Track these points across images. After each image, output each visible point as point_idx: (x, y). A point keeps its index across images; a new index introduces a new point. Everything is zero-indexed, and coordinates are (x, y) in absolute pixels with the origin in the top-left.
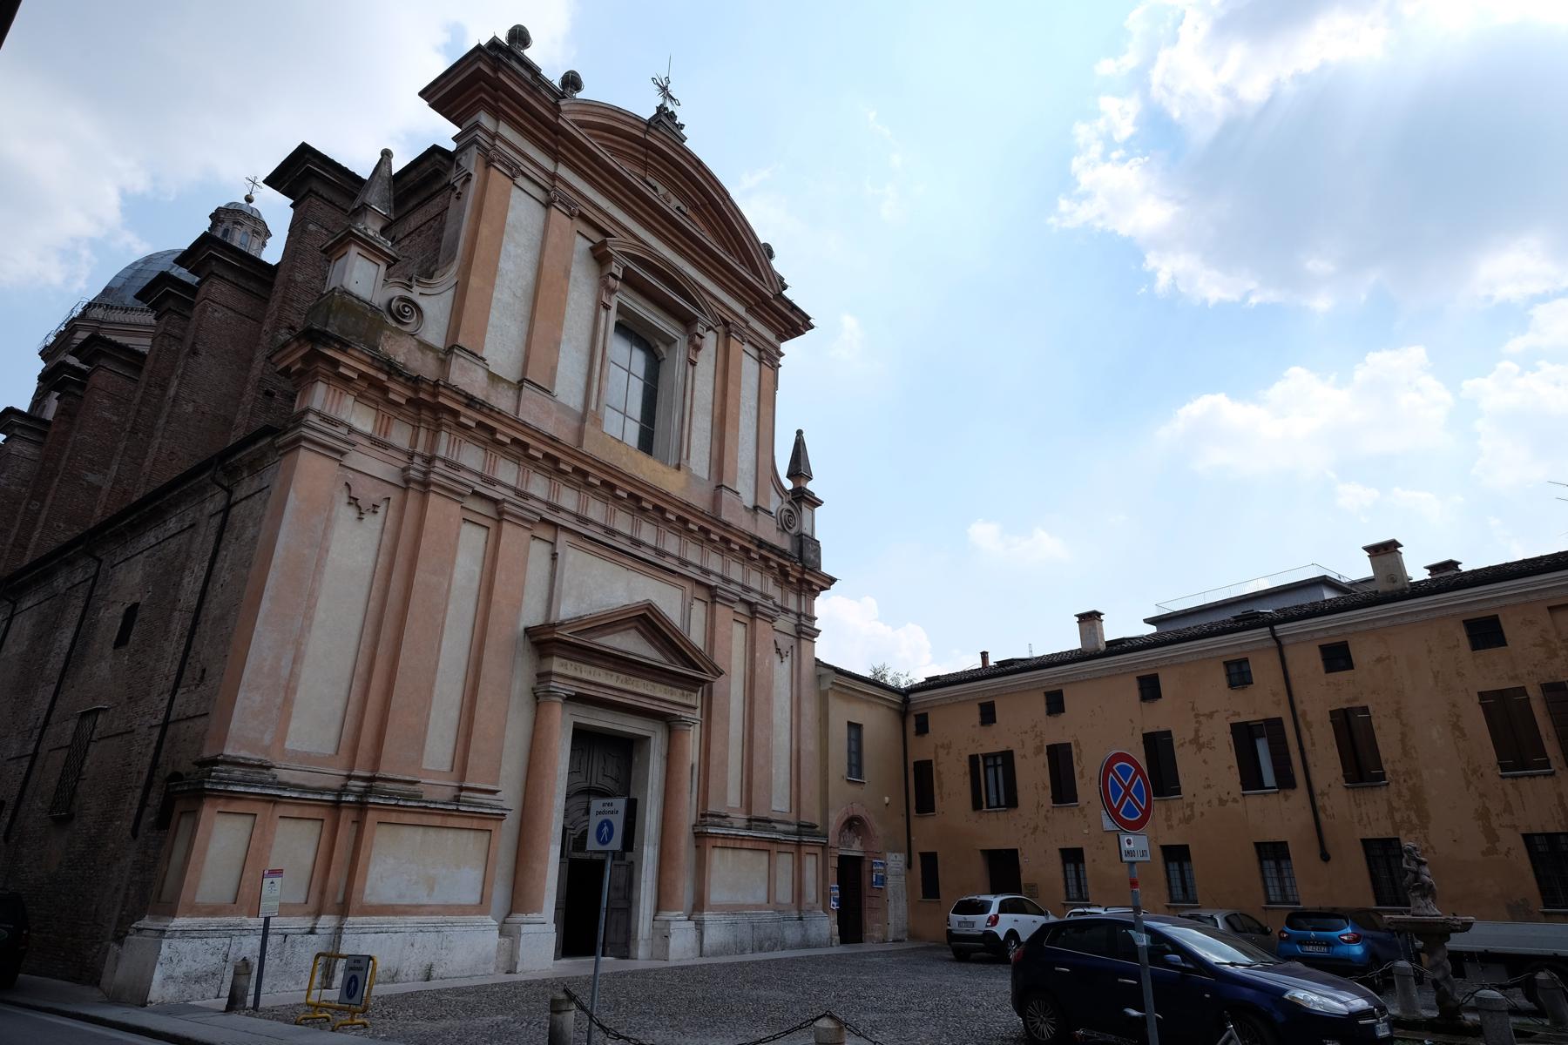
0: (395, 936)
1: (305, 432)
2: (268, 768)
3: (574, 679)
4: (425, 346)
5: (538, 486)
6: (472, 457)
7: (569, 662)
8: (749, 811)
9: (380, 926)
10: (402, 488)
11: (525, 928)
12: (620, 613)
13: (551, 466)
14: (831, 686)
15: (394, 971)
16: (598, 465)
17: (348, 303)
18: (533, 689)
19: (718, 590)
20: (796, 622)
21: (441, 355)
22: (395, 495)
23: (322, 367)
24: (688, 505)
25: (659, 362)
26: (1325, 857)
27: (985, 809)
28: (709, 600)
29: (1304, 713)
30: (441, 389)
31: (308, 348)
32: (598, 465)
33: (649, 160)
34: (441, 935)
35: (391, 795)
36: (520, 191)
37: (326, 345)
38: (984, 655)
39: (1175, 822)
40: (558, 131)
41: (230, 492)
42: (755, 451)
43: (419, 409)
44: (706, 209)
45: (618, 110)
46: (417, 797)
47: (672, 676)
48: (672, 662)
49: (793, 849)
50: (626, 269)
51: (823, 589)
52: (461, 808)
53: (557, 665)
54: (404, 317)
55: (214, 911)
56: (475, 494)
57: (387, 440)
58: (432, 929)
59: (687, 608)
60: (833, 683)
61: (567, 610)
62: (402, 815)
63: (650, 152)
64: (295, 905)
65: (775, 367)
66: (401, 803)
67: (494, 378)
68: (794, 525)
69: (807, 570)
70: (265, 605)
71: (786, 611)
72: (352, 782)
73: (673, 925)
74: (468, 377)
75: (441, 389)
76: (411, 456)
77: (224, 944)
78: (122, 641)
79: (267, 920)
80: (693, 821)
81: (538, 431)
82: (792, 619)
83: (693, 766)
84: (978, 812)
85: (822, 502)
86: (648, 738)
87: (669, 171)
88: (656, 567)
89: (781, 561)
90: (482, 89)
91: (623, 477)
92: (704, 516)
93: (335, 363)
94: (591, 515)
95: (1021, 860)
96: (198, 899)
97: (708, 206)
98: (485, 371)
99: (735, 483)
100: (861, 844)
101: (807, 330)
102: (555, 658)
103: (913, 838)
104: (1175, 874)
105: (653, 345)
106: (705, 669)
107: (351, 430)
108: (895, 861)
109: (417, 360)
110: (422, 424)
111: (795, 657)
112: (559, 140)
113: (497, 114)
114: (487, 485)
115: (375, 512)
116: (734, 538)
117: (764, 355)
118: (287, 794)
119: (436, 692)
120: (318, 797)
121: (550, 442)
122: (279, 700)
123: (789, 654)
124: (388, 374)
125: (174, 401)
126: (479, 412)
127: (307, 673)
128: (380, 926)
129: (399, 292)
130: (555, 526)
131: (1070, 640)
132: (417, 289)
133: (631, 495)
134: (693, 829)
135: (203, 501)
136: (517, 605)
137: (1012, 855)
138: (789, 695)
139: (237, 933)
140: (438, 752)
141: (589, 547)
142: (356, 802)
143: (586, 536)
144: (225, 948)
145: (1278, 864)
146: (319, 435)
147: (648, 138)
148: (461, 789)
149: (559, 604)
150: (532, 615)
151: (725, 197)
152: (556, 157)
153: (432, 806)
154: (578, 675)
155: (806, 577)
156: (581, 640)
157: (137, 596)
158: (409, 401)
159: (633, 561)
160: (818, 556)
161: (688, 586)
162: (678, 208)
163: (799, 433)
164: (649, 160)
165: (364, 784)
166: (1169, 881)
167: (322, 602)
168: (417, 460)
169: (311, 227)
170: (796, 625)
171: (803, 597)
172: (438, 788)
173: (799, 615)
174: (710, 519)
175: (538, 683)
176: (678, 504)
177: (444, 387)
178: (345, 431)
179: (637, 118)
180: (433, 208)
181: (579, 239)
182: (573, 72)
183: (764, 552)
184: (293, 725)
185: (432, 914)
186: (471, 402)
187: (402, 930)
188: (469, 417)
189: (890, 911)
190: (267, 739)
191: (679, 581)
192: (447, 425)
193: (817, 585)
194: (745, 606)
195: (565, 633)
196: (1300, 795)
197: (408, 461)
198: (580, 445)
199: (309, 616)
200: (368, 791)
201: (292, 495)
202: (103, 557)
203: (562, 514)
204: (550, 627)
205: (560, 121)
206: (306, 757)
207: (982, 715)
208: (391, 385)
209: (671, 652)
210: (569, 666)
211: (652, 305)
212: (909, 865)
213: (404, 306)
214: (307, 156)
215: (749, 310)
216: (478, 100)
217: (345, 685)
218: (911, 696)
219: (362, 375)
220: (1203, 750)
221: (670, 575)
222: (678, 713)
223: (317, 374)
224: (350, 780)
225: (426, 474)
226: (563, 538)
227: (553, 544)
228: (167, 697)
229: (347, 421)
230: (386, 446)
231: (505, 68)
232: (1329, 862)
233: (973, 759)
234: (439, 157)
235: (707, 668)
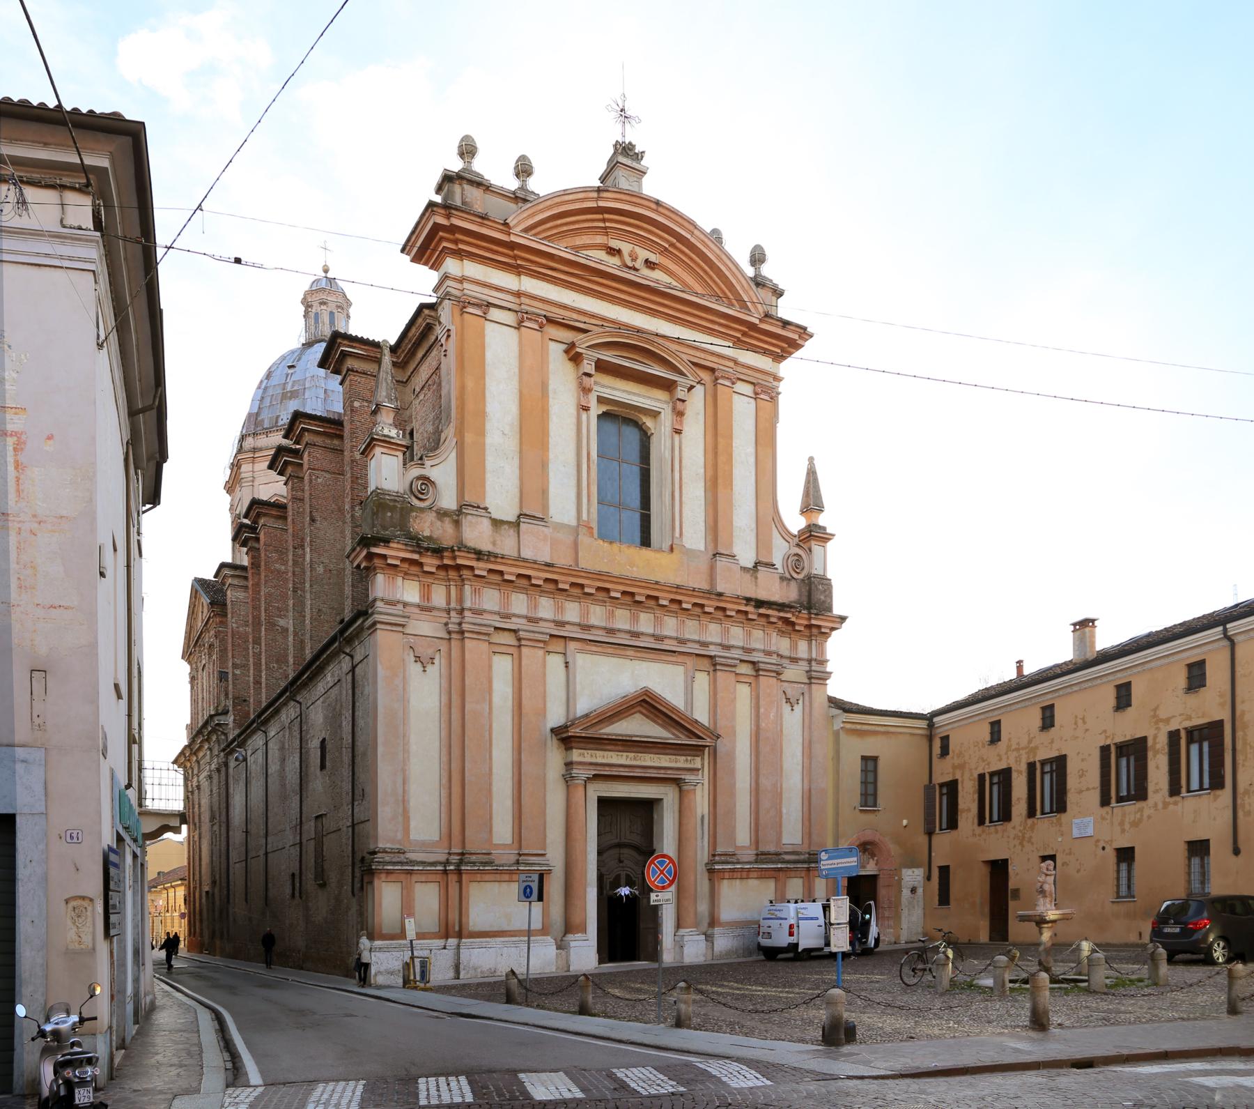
0: (491, 950)
1: (377, 617)
2: (404, 853)
3: (591, 764)
4: (442, 514)
5: (546, 608)
6: (490, 599)
7: (585, 752)
8: (757, 848)
11: (572, 944)
12: (621, 704)
13: (553, 587)
14: (842, 725)
15: (493, 970)
16: (590, 576)
17: (381, 503)
18: (563, 775)
20: (808, 669)
21: (455, 518)
22: (443, 646)
23: (377, 562)
24: (678, 587)
25: (649, 437)
26: (1236, 851)
27: (1184, 794)
28: (711, 669)
29: (1243, 713)
30: (457, 553)
31: (364, 553)
32: (590, 576)
35: (474, 863)
36: (493, 324)
37: (375, 545)
38: (1020, 665)
39: (1127, 826)
41: (352, 657)
42: (754, 501)
43: (447, 571)
44: (676, 248)
45: (565, 192)
46: (490, 863)
47: (674, 747)
49: (803, 874)
51: (833, 629)
52: (520, 868)
53: (576, 755)
57: (429, 605)
59: (690, 682)
60: (844, 722)
61: (583, 706)
62: (483, 876)
64: (433, 933)
65: (773, 397)
66: (481, 868)
67: (497, 523)
68: (803, 569)
69: (813, 616)
70: (380, 749)
71: (794, 660)
72: (452, 857)
73: (686, 938)
74: (477, 533)
75: (457, 553)
76: (448, 611)
78: (323, 767)
79: (411, 941)
80: (706, 860)
81: (535, 562)
82: (804, 666)
83: (703, 817)
84: (981, 827)
85: (834, 535)
86: (662, 799)
88: (657, 651)
89: (782, 614)
90: (442, 239)
91: (615, 580)
92: (695, 593)
94: (594, 621)
95: (1010, 868)
96: (384, 932)
98: (488, 519)
99: (731, 545)
100: (876, 865)
102: (574, 750)
103: (933, 854)
104: (1124, 874)
105: (640, 423)
107: (405, 604)
108: (913, 876)
109: (438, 529)
110: (451, 583)
111: (807, 703)
113: (459, 254)
114: (505, 620)
118: (416, 868)
119: (494, 789)
120: (433, 868)
121: (547, 568)
122: (401, 810)
123: (800, 702)
124: (420, 553)
125: (311, 567)
126: (488, 561)
127: (413, 788)
129: (415, 472)
131: (1064, 652)
132: (428, 463)
133: (624, 593)
135: (340, 662)
136: (542, 713)
137: (1005, 862)
138: (801, 740)
140: (503, 831)
141: (594, 649)
142: (455, 870)
145: (1202, 859)
146: (386, 617)
148: (520, 855)
149: (575, 705)
150: (556, 717)
151: (691, 228)
152: (517, 270)
153: (501, 868)
154: (594, 760)
155: (814, 622)
156: (591, 733)
157: (323, 735)
158: (439, 567)
160: (830, 596)
161: (690, 662)
163: (811, 459)
165: (458, 858)
166: (1118, 879)
167: (413, 738)
168: (453, 614)
169: (356, 404)
170: (807, 672)
171: (814, 642)
172: (506, 857)
173: (810, 661)
174: (702, 594)
175: (567, 770)
176: (668, 589)
177: (459, 551)
178: (400, 607)
179: (585, 190)
180: (431, 362)
181: (552, 345)
183: (762, 611)
184: (413, 824)
186: (479, 555)
188: (481, 568)
189: (903, 918)
190: (399, 836)
191: (681, 659)
192: (469, 580)
193: (826, 627)
196: (1225, 795)
198: (577, 565)
199: (406, 751)
200: (461, 862)
201: (380, 668)
202: (301, 700)
204: (572, 723)
206: (423, 843)
207: (1190, 678)
208: (423, 560)
209: (674, 728)
210: (586, 754)
211: (631, 384)
212: (929, 878)
214: (339, 341)
216: (441, 252)
217: (438, 794)
218: (935, 720)
219: (403, 560)
220: (1158, 756)
221: (672, 656)
222: (683, 777)
223: (375, 569)
225: (460, 624)
226: (572, 646)
228: (350, 806)
229: (401, 599)
230: (429, 609)
231: (453, 212)
232: (1240, 856)
233: (1105, 750)
234: (426, 312)
235: (705, 734)
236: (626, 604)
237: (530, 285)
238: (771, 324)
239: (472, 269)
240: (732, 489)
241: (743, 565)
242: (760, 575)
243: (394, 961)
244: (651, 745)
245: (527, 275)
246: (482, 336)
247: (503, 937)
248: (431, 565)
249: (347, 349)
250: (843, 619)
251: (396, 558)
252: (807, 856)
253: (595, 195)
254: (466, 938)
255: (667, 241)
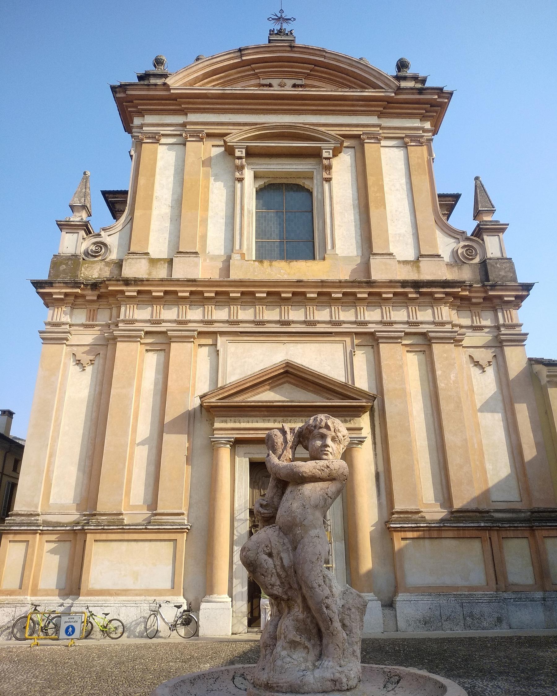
7: (228, 419)
9: (97, 602)
10: (499, 347)
14: (548, 379)
19: (377, 334)
24: (322, 282)
33: (256, 71)
34: (139, 609)
40: (175, 98)
48: (328, 399)
50: (247, 148)
54: (98, 252)
55: (11, 593)
56: (407, 334)
58: (133, 605)
63: (253, 66)
66: (106, 528)
77: (12, 611)
87: (276, 67)
92: (342, 284)
93: (500, 297)
97: (316, 68)
101: (449, 99)
106: (359, 398)
109: (106, 272)
112: (180, 101)
113: (141, 113)
115: (490, 365)
116: (434, 290)
117: (407, 140)
128: (97, 602)
130: (215, 333)
134: (386, 525)
139: (19, 605)
143: (241, 332)
144: (13, 613)
147: (244, 58)
152: (184, 112)
156: (238, 400)
158: (485, 299)
159: (288, 337)
162: (294, 86)
163: (477, 178)
164: (256, 71)
182: (402, 59)
185: (137, 595)
187: (112, 605)
188: (131, 291)
194: (421, 337)
195: (213, 400)
197: (497, 331)
203: (216, 325)
205: (172, 91)
209: (327, 393)
211: (283, 159)
213: (467, 250)
215: (381, 115)
224: (533, 513)
226: (221, 340)
227: (215, 345)
231: (128, 87)
236: (276, 302)
237: (192, 117)
238: (404, 94)
239: (149, 119)
240: (385, 208)
241: (401, 259)
242: (421, 264)
243: (5, 617)
244: (299, 409)
245: (191, 112)
246: (155, 153)
247: (125, 595)
248: (93, 295)
249: (112, 199)
250: (528, 287)
251: (60, 293)
252: (529, 513)
253: (239, 54)
254: (84, 596)
255: (306, 69)
